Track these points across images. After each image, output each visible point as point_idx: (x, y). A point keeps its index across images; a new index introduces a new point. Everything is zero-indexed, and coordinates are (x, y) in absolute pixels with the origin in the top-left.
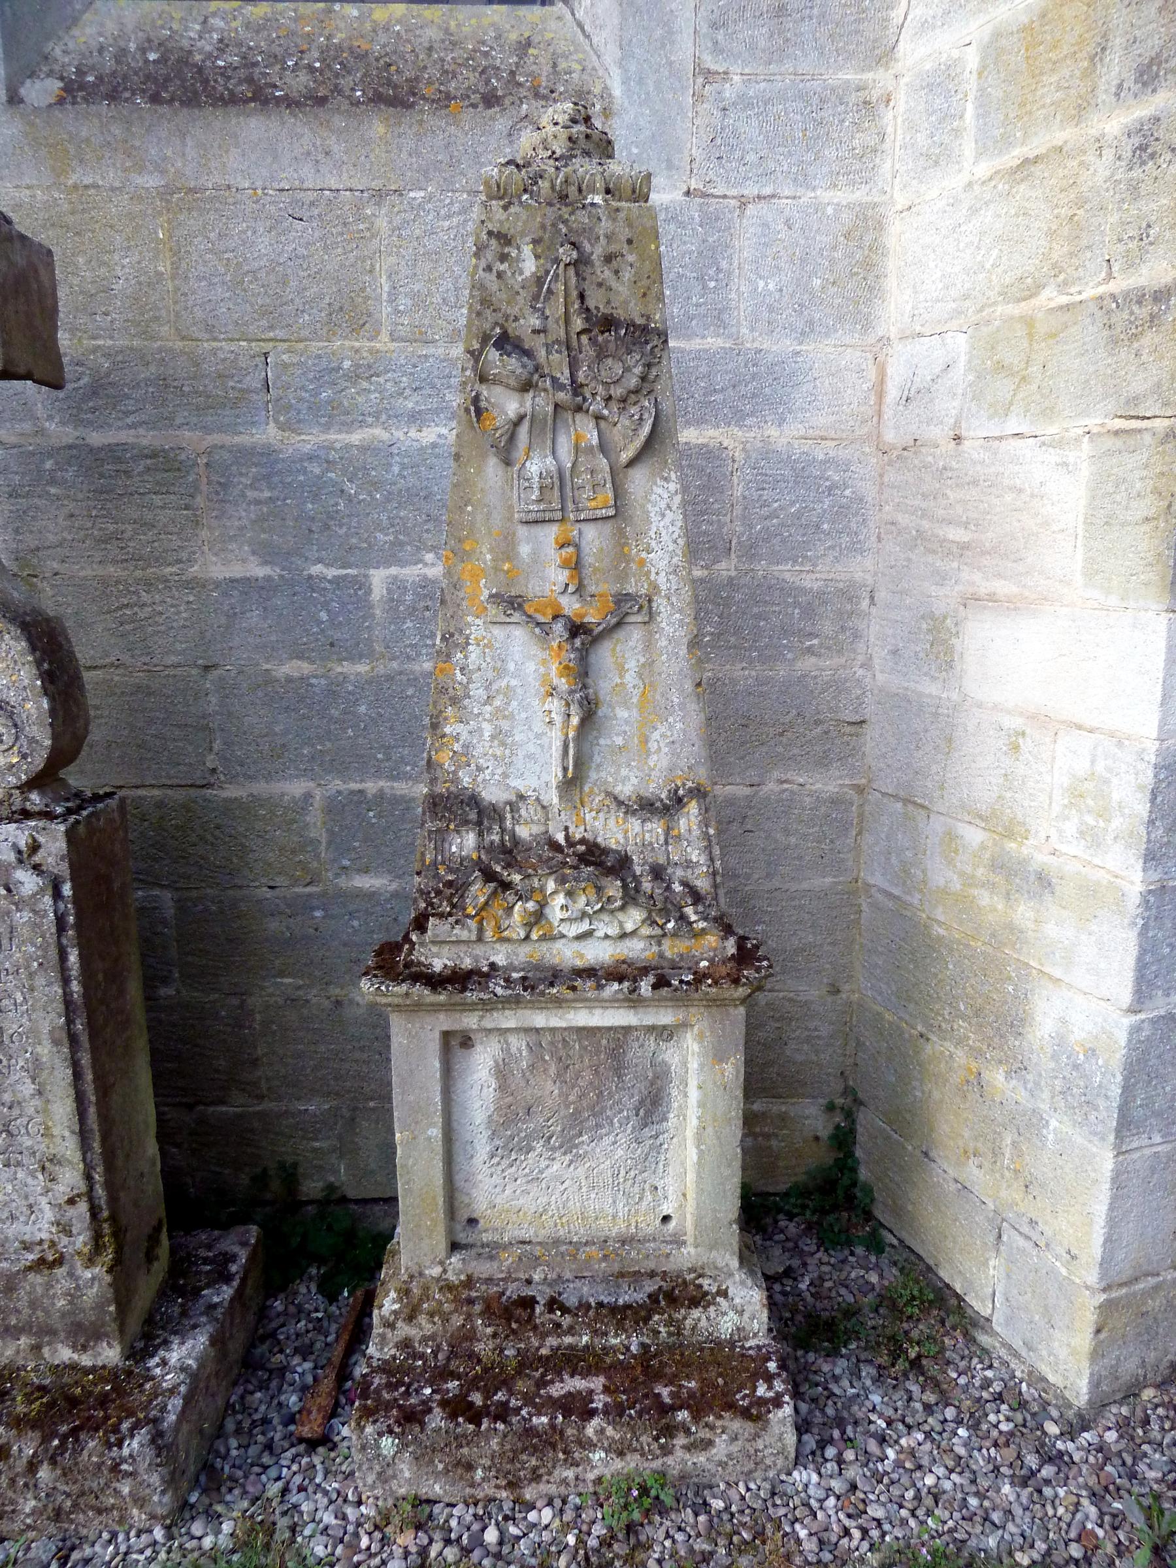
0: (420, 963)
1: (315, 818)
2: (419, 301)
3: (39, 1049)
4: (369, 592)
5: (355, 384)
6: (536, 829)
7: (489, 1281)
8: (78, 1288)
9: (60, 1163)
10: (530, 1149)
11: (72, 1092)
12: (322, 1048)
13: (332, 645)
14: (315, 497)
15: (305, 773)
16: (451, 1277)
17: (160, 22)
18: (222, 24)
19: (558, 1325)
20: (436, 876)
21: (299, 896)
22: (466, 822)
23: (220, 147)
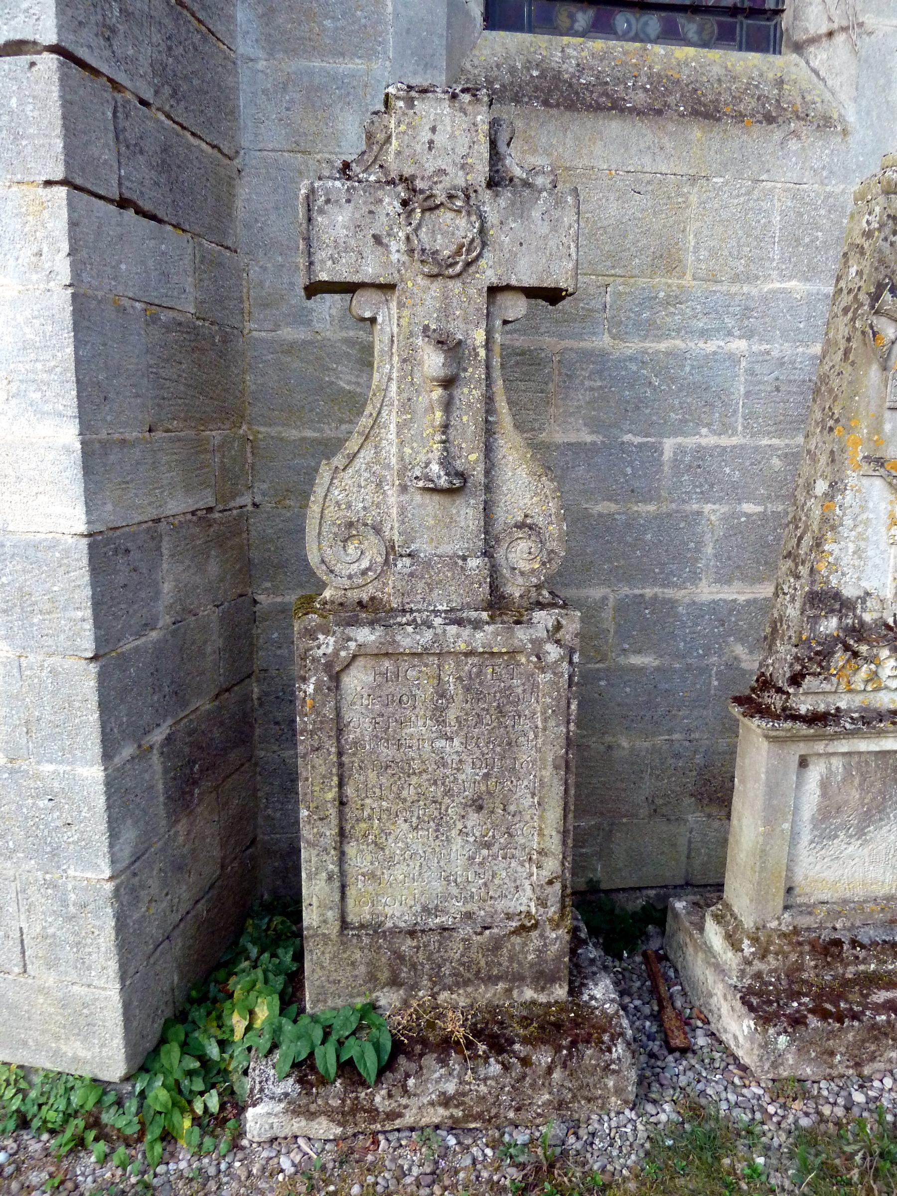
0: (791, 709)
1: (608, 614)
2: (713, 253)
3: (544, 772)
4: (662, 454)
5: (666, 309)
6: (876, 615)
7: (808, 929)
8: (545, 945)
9: (546, 854)
10: (836, 837)
11: (562, 803)
12: (594, 781)
13: (633, 491)
14: (632, 387)
15: (603, 583)
16: (784, 928)
17: (532, 50)
18: (575, 53)
19: (857, 958)
20: (810, 647)
21: (591, 670)
22: (832, 611)
23: (590, 140)
